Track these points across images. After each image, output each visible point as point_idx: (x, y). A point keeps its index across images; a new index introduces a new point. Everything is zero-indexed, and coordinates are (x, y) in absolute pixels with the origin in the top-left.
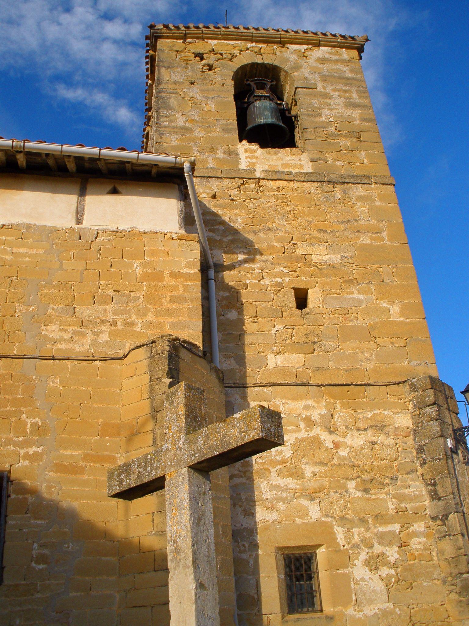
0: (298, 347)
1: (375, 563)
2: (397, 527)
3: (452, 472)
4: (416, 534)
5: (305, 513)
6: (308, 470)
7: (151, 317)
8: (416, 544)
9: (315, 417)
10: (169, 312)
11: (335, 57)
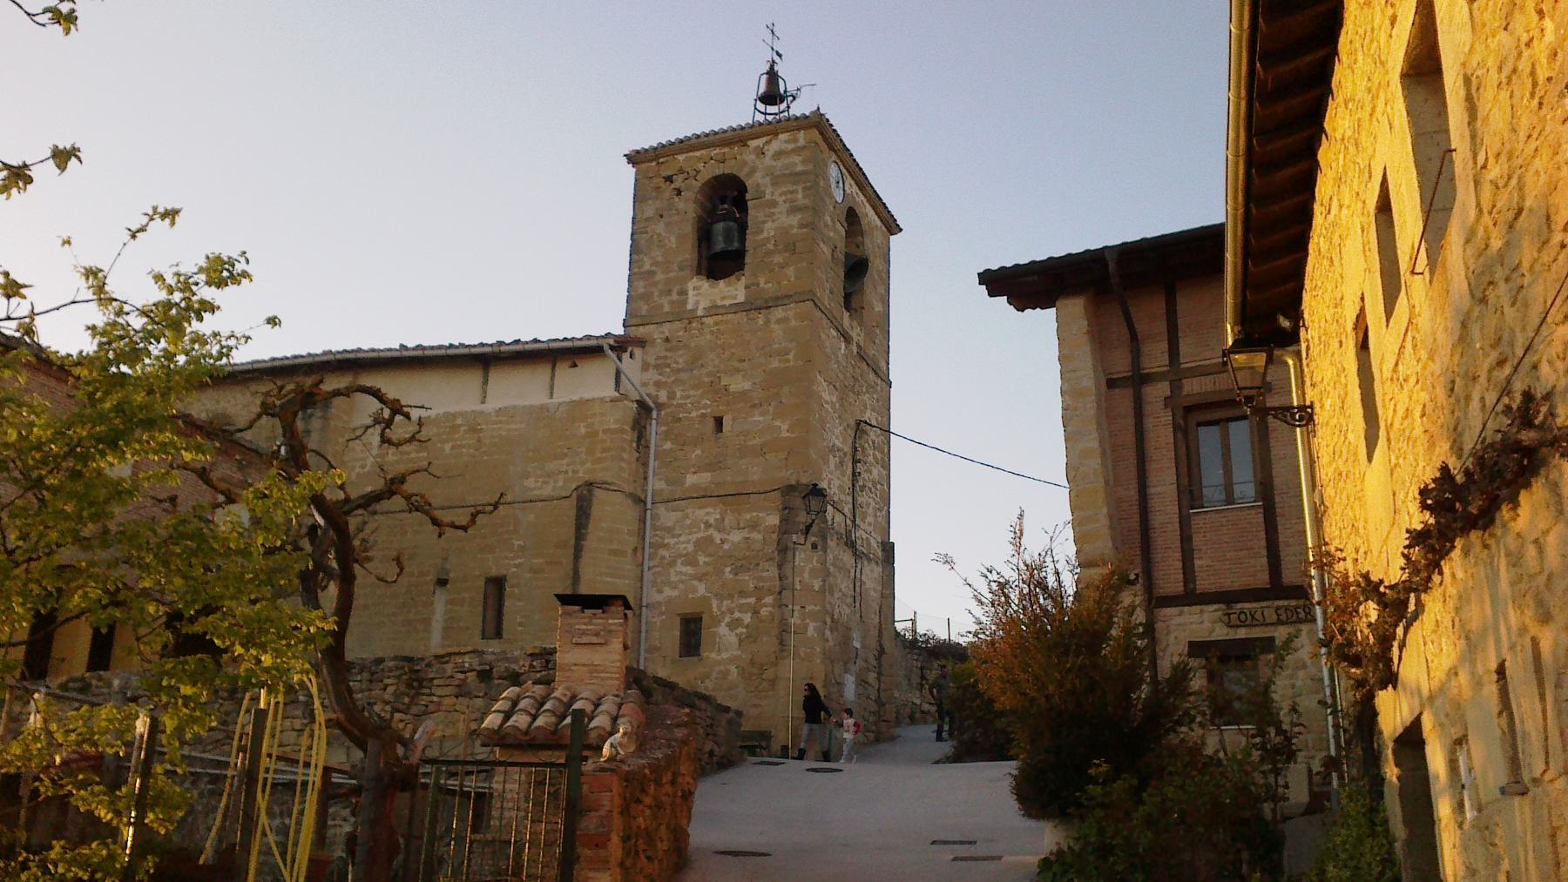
0: (709, 467)
1: (733, 625)
2: (752, 600)
3: (1409, 345)
4: (765, 605)
5: (695, 590)
6: (702, 559)
7: (588, 465)
8: (764, 612)
9: (712, 521)
10: (600, 460)
11: (791, 146)
